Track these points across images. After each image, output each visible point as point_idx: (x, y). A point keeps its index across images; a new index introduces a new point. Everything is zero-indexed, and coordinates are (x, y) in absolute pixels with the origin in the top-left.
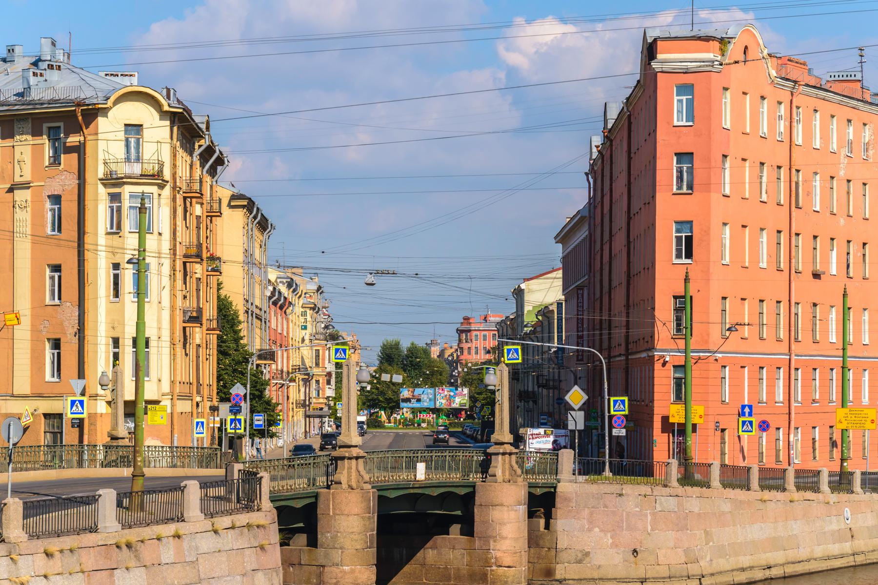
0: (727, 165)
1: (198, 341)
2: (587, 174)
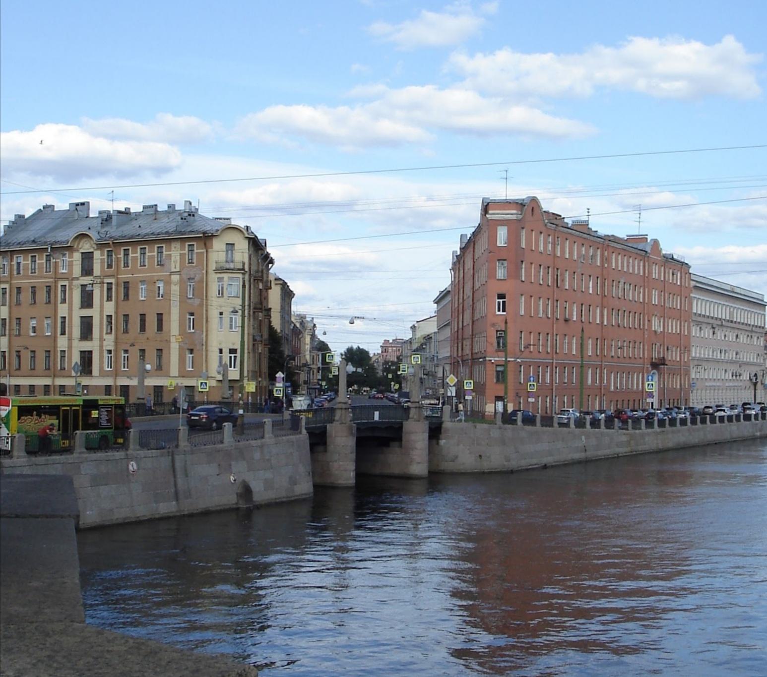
0: (523, 266)
1: (260, 351)
2: (451, 270)
